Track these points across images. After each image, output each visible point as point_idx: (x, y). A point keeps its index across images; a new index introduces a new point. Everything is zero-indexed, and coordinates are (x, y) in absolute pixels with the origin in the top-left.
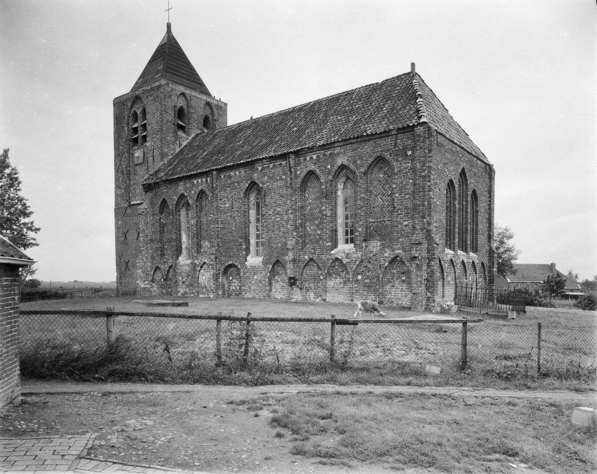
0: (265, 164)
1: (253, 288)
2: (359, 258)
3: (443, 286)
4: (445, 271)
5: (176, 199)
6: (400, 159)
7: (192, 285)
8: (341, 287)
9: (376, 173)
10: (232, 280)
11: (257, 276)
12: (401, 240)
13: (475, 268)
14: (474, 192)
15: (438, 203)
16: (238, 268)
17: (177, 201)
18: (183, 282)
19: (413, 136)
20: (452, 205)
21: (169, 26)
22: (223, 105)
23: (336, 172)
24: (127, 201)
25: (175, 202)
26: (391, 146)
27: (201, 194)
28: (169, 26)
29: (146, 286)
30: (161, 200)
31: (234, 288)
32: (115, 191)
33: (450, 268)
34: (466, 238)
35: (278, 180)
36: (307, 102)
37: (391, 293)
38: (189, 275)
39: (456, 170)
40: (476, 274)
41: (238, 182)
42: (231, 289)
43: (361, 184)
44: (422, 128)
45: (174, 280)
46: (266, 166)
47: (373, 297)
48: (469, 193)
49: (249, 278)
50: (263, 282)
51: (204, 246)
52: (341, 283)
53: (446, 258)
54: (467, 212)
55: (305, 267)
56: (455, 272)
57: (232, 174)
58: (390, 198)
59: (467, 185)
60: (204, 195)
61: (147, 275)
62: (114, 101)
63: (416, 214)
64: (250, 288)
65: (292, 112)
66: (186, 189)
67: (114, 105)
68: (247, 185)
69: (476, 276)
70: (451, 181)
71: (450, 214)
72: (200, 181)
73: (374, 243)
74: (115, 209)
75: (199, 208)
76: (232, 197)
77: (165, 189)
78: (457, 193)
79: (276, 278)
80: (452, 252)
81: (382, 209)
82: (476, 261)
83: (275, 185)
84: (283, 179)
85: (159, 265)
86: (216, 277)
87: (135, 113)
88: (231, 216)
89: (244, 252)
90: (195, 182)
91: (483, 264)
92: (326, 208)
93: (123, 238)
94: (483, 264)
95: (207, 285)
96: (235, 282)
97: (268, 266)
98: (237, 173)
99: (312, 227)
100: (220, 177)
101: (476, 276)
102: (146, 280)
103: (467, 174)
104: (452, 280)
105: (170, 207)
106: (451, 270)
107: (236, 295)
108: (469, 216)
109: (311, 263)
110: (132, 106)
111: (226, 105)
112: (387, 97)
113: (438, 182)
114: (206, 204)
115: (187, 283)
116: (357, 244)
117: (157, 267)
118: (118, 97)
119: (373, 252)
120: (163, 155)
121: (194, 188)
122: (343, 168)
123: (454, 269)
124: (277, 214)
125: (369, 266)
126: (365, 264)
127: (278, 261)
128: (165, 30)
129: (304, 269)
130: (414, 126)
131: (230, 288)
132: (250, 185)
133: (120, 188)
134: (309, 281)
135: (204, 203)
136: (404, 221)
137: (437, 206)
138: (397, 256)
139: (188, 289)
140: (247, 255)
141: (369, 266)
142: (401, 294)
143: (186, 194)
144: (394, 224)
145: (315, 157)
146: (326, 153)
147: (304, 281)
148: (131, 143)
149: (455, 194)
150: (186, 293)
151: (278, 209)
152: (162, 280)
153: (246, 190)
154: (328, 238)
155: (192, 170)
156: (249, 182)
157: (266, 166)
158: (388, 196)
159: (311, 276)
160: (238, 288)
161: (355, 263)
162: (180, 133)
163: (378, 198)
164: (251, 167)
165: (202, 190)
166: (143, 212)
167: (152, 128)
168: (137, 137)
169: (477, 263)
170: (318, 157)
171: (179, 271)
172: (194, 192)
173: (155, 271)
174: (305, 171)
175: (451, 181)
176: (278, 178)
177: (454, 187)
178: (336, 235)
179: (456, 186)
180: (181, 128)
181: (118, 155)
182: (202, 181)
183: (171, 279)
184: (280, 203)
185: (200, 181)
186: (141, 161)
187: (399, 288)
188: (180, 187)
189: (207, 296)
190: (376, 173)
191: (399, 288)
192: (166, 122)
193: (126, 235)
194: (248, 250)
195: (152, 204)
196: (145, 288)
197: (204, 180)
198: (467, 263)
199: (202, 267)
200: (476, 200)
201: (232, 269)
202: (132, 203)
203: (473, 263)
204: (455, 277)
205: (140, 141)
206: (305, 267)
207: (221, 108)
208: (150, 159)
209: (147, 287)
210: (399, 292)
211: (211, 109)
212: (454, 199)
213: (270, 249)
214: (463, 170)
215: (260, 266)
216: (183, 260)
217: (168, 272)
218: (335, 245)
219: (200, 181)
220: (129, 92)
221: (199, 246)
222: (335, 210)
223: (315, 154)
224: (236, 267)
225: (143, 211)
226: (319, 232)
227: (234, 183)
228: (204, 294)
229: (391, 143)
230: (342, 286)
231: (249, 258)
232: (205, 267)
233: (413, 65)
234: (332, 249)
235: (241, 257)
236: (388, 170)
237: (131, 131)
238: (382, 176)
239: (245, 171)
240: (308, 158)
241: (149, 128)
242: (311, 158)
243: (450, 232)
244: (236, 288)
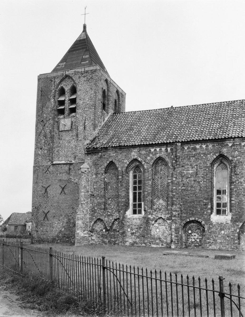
0: (237, 142)
1: (219, 241)
7: (144, 236)
10: (191, 234)
11: (225, 232)
21: (85, 27)
23: (155, 161)
24: (50, 160)
27: (158, 159)
28: (85, 27)
29: (85, 235)
30: (108, 162)
31: (193, 240)
32: (35, 151)
36: (233, 100)
38: (141, 228)
46: (238, 143)
49: (214, 233)
50: (232, 237)
51: (158, 204)
61: (87, 225)
62: (39, 76)
64: (215, 240)
68: (215, 157)
74: (34, 167)
77: (114, 153)
88: (195, 181)
93: (44, 192)
95: (161, 237)
96: (195, 236)
100: (184, 148)
102: (85, 230)
105: (119, 169)
107: (196, 246)
110: (60, 83)
114: (161, 169)
115: (138, 234)
118: (44, 74)
120: (95, 126)
122: (159, 159)
128: (82, 29)
133: (41, 149)
139: (138, 240)
140: (211, 213)
148: (56, 113)
150: (135, 242)
153: (214, 161)
156: (217, 155)
157: (238, 143)
160: (198, 240)
166: (86, 171)
167: (83, 103)
171: (128, 224)
172: (151, 159)
183: (115, 230)
186: (67, 128)
188: (133, 153)
189: (161, 246)
193: (46, 189)
195: (95, 164)
196: (84, 237)
199: (156, 221)
202: (54, 163)
208: (81, 128)
209: (86, 236)
213: (240, 210)
215: (228, 223)
217: (113, 224)
220: (50, 72)
225: (85, 170)
227: (199, 153)
228: (158, 244)
235: (206, 215)
237: (57, 104)
239: (213, 146)
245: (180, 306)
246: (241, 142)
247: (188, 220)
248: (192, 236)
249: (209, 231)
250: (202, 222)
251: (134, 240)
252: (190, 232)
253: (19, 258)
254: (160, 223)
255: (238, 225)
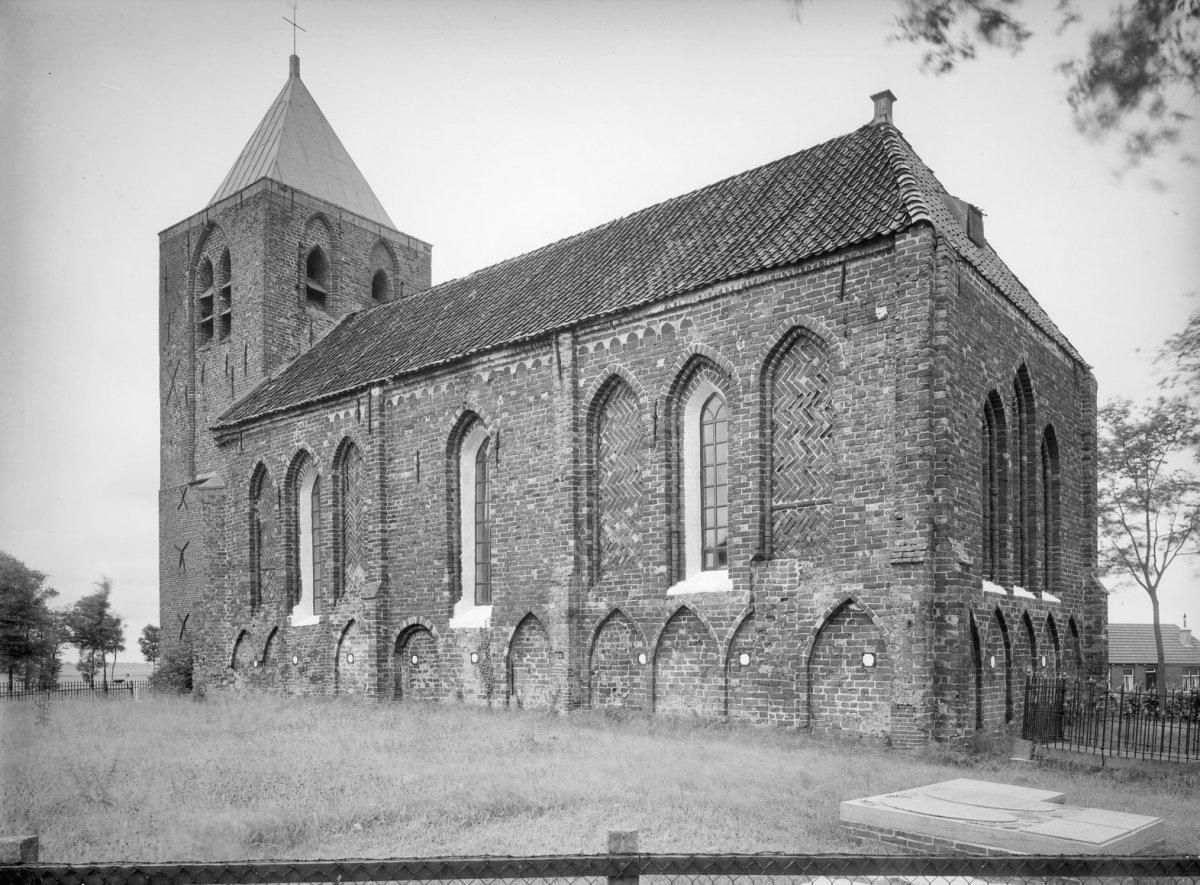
2: (743, 606)
3: (979, 684)
4: (982, 642)
5: (288, 463)
6: (855, 331)
8: (695, 687)
9: (787, 375)
10: (416, 665)
12: (860, 554)
13: (1055, 633)
14: (1049, 430)
15: (962, 451)
16: (431, 635)
17: (291, 468)
18: (302, 671)
19: (893, 265)
20: (996, 461)
21: (295, 61)
22: (421, 248)
25: (285, 471)
26: (830, 297)
28: (295, 61)
31: (423, 686)
33: (995, 633)
34: (1032, 553)
35: (530, 405)
37: (833, 704)
39: (1005, 367)
40: (1057, 648)
41: (431, 413)
42: (416, 687)
43: (747, 404)
44: (917, 239)
45: (281, 665)
47: (781, 713)
48: (1036, 432)
52: (695, 674)
53: (983, 607)
54: (1032, 483)
55: (598, 630)
56: (1007, 645)
57: (418, 393)
58: (827, 441)
59: (1031, 411)
60: (353, 451)
63: (905, 481)
65: (576, 244)
66: (310, 436)
67: (161, 247)
68: (454, 421)
69: (1058, 655)
70: (994, 396)
71: (992, 486)
72: (342, 416)
73: (785, 564)
75: (340, 484)
76: (418, 453)
78: (1009, 430)
79: (525, 660)
80: (1030, 595)
81: (806, 472)
82: (1058, 616)
83: (522, 417)
84: (543, 401)
85: (247, 627)
86: (380, 655)
87: (208, 265)
89: (446, 594)
90: (332, 417)
91: (1072, 622)
92: (654, 472)
94: (1072, 622)
96: (426, 671)
97: (505, 629)
98: (431, 391)
99: (617, 525)
101: (1058, 655)
103: (1032, 382)
104: (1001, 665)
105: (274, 484)
106: (997, 639)
108: (1040, 494)
109: (616, 621)
111: (428, 247)
112: (818, 179)
113: (962, 393)
116: (735, 570)
117: (244, 632)
119: (781, 589)
121: (329, 434)
123: (1006, 637)
124: (529, 492)
125: (771, 626)
126: (759, 624)
127: (530, 615)
128: (284, 76)
129: (596, 637)
130: (894, 232)
131: (412, 686)
132: (461, 420)
134: (610, 668)
135: (352, 472)
136: (866, 502)
137: (961, 459)
138: (850, 601)
141: (771, 626)
142: (861, 706)
143: (310, 450)
144: (841, 511)
145: (623, 339)
146: (653, 327)
147: (597, 668)
149: (1004, 433)
151: (531, 481)
152: (256, 664)
154: (659, 552)
155: (327, 389)
156: (459, 413)
158: (822, 437)
159: (616, 656)
161: (733, 619)
162: (313, 310)
163: (793, 442)
164: (464, 373)
165: (346, 439)
168: (212, 319)
169: (1060, 621)
170: (633, 337)
173: (239, 640)
174: (599, 379)
175: (994, 396)
176: (531, 399)
177: (1000, 414)
178: (680, 543)
179: (1008, 411)
180: (317, 298)
181: (169, 368)
182: (347, 414)
184: (534, 465)
185: (342, 416)
187: (856, 691)
190: (787, 375)
191: (856, 691)
192: (274, 280)
193: (182, 554)
194: (456, 589)
197: (352, 412)
198: (1036, 619)
199: (345, 632)
200: (1054, 454)
201: (419, 636)
203: (1050, 619)
204: (1008, 657)
205: (216, 331)
206: (598, 630)
207: (419, 254)
210: (856, 701)
211: (392, 255)
212: (1002, 446)
214: (1022, 370)
216: (304, 615)
218: (677, 573)
219: (342, 414)
221: (339, 576)
222: (679, 478)
223: (625, 331)
224: (427, 630)
226: (636, 538)
229: (830, 290)
230: (697, 681)
231: (458, 607)
232: (353, 631)
233: (885, 99)
234: (671, 584)
236: (820, 364)
238: (803, 380)
240: (607, 343)
241: (235, 296)
242: (615, 342)
243: (991, 536)
244: (427, 685)
245: (1115, 738)
246: (614, 334)
247: (405, 626)
248: (420, 672)
249: (446, 655)
250: (431, 627)
251: (304, 689)
252: (415, 660)
253: (1046, 513)
254: (354, 638)
255: (506, 635)
